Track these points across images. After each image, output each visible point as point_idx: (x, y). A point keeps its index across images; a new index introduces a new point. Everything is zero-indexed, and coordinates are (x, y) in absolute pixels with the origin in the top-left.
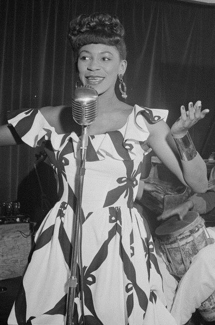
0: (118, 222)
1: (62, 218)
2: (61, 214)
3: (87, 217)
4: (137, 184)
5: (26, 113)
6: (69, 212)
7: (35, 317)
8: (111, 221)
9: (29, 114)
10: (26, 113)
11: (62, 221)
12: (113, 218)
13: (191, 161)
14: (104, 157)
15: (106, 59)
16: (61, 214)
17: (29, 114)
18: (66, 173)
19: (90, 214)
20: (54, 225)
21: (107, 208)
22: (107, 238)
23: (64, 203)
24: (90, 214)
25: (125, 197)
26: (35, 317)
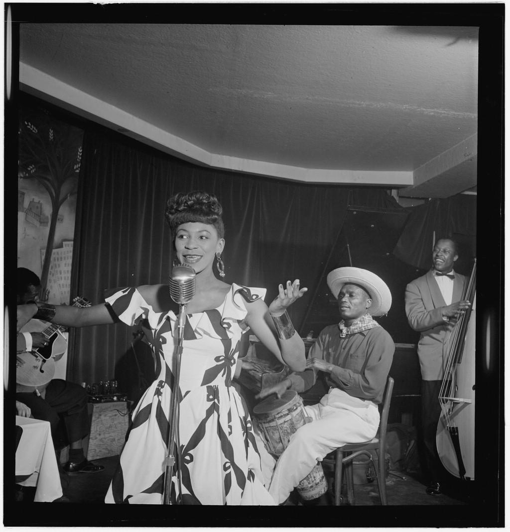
0: (216, 401)
1: (160, 397)
2: (158, 393)
3: (185, 396)
4: (235, 363)
5: (124, 292)
6: (167, 390)
7: (189, 392)
8: (209, 400)
9: (126, 293)
10: (124, 292)
11: (159, 400)
12: (211, 397)
13: (289, 340)
14: (201, 335)
15: (184, 237)
16: (158, 393)
17: (126, 293)
18: (164, 352)
19: (187, 393)
20: (151, 404)
21: (205, 387)
22: (204, 416)
23: (161, 382)
24: (187, 393)
25: (223, 376)
26: (189, 392)
